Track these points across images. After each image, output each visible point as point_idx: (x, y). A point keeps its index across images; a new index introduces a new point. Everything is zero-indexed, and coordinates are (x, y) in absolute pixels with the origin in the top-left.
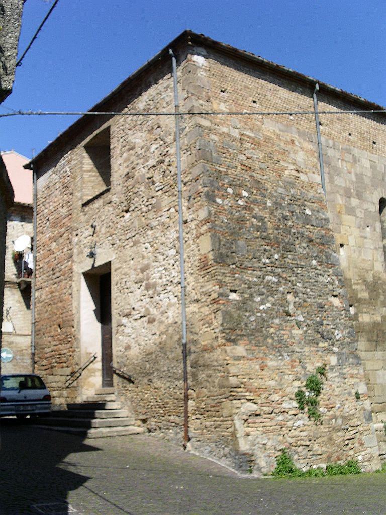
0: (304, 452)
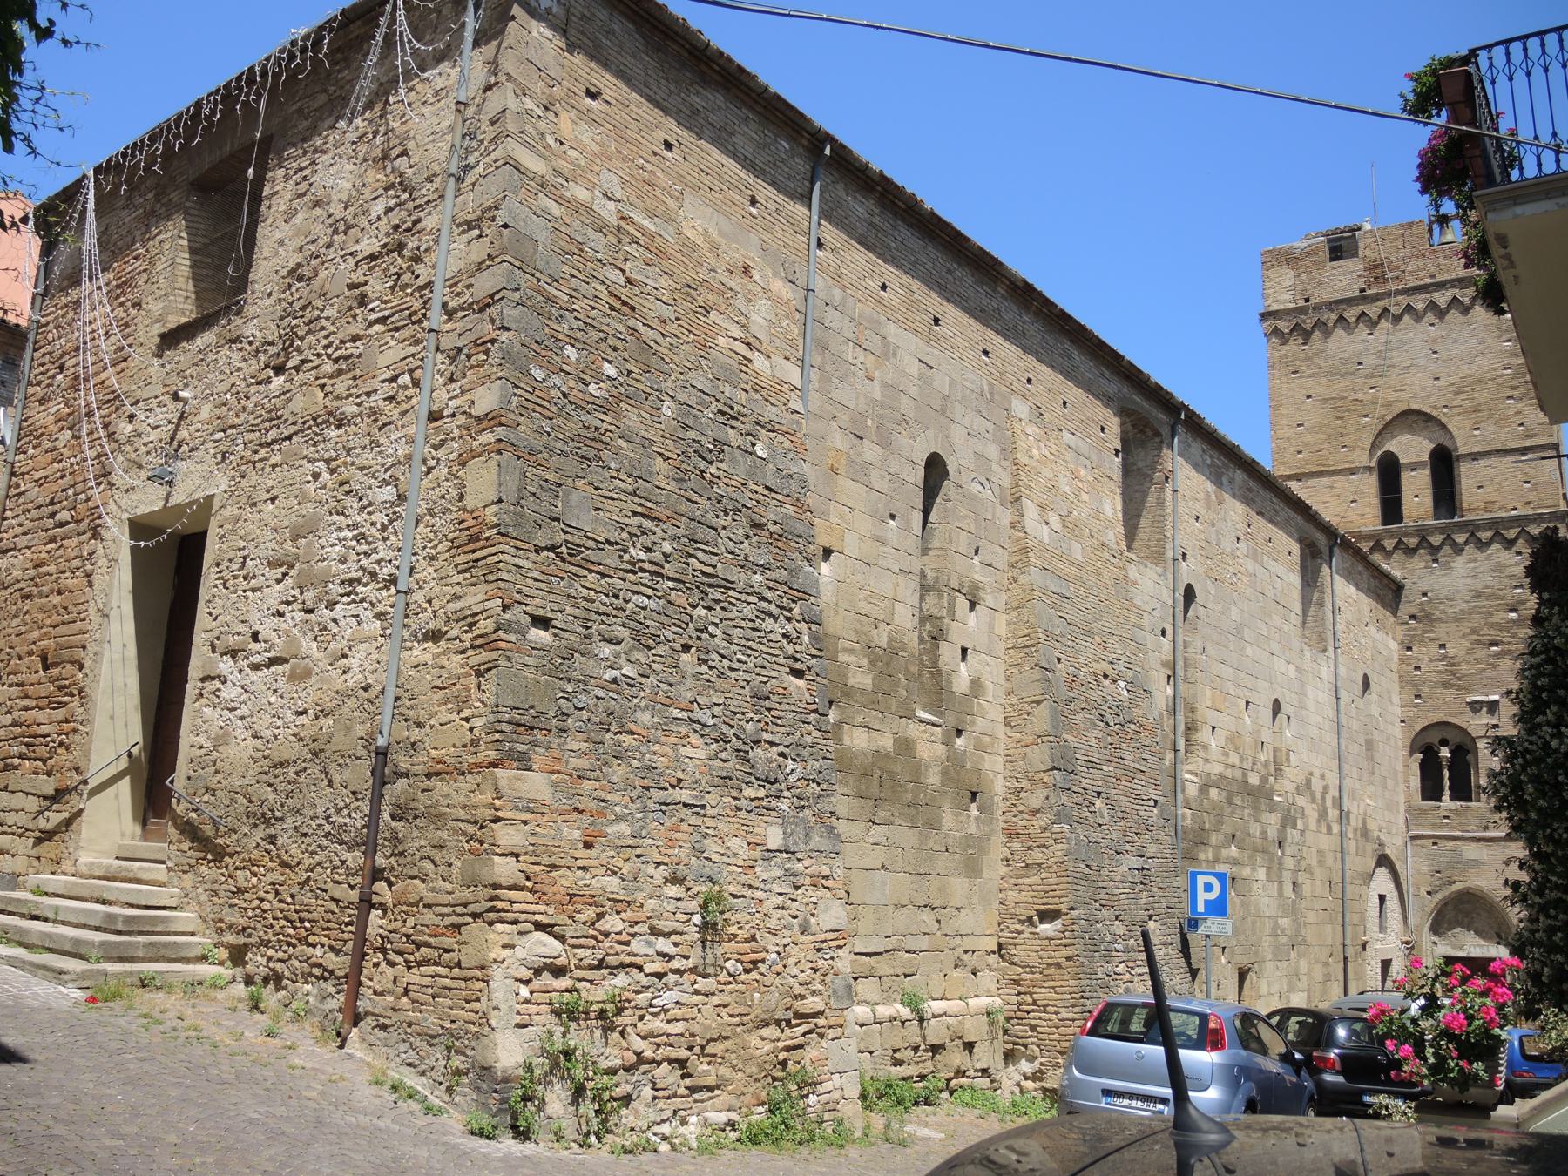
0: (670, 1080)
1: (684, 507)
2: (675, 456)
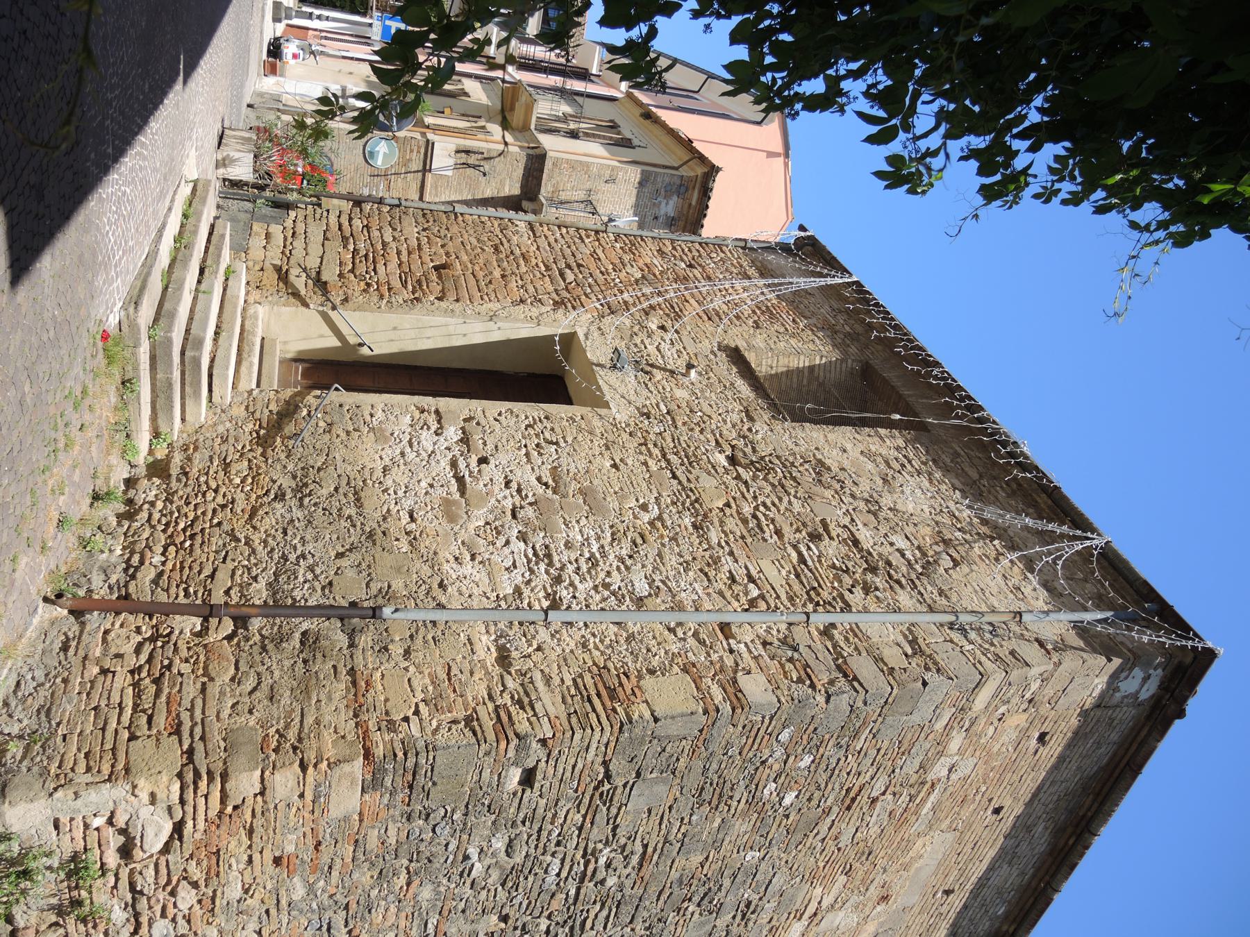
1: (653, 890)
2: (704, 872)
